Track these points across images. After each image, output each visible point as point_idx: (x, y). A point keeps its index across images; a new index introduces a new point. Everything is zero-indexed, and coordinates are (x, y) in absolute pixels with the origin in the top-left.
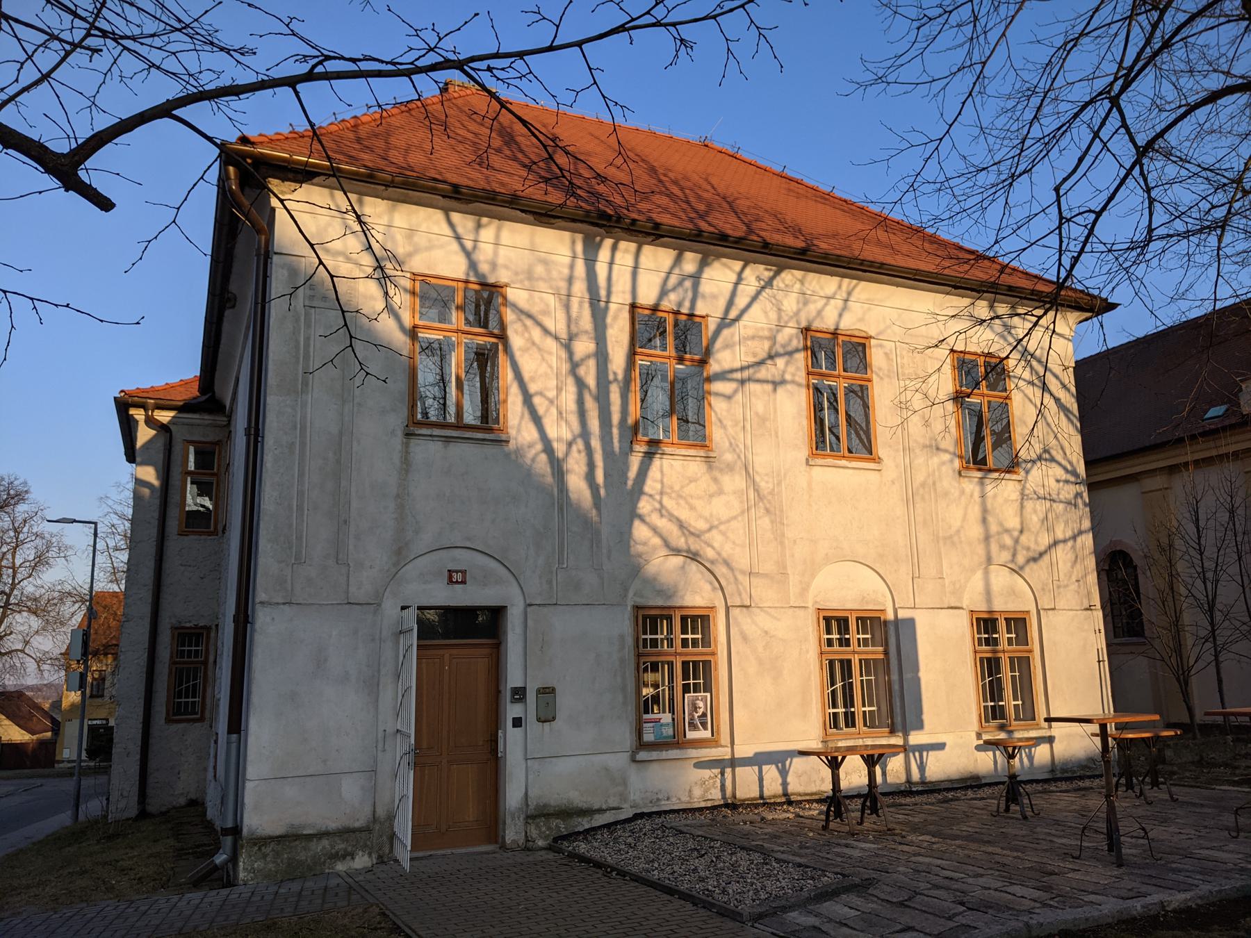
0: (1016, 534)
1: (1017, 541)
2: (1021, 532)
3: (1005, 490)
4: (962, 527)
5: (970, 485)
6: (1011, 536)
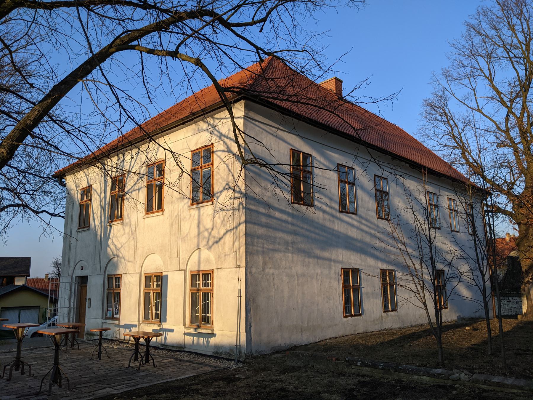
0: (210, 230)
1: (210, 234)
2: (212, 229)
3: (207, 209)
4: (189, 232)
5: (194, 212)
6: (208, 232)
